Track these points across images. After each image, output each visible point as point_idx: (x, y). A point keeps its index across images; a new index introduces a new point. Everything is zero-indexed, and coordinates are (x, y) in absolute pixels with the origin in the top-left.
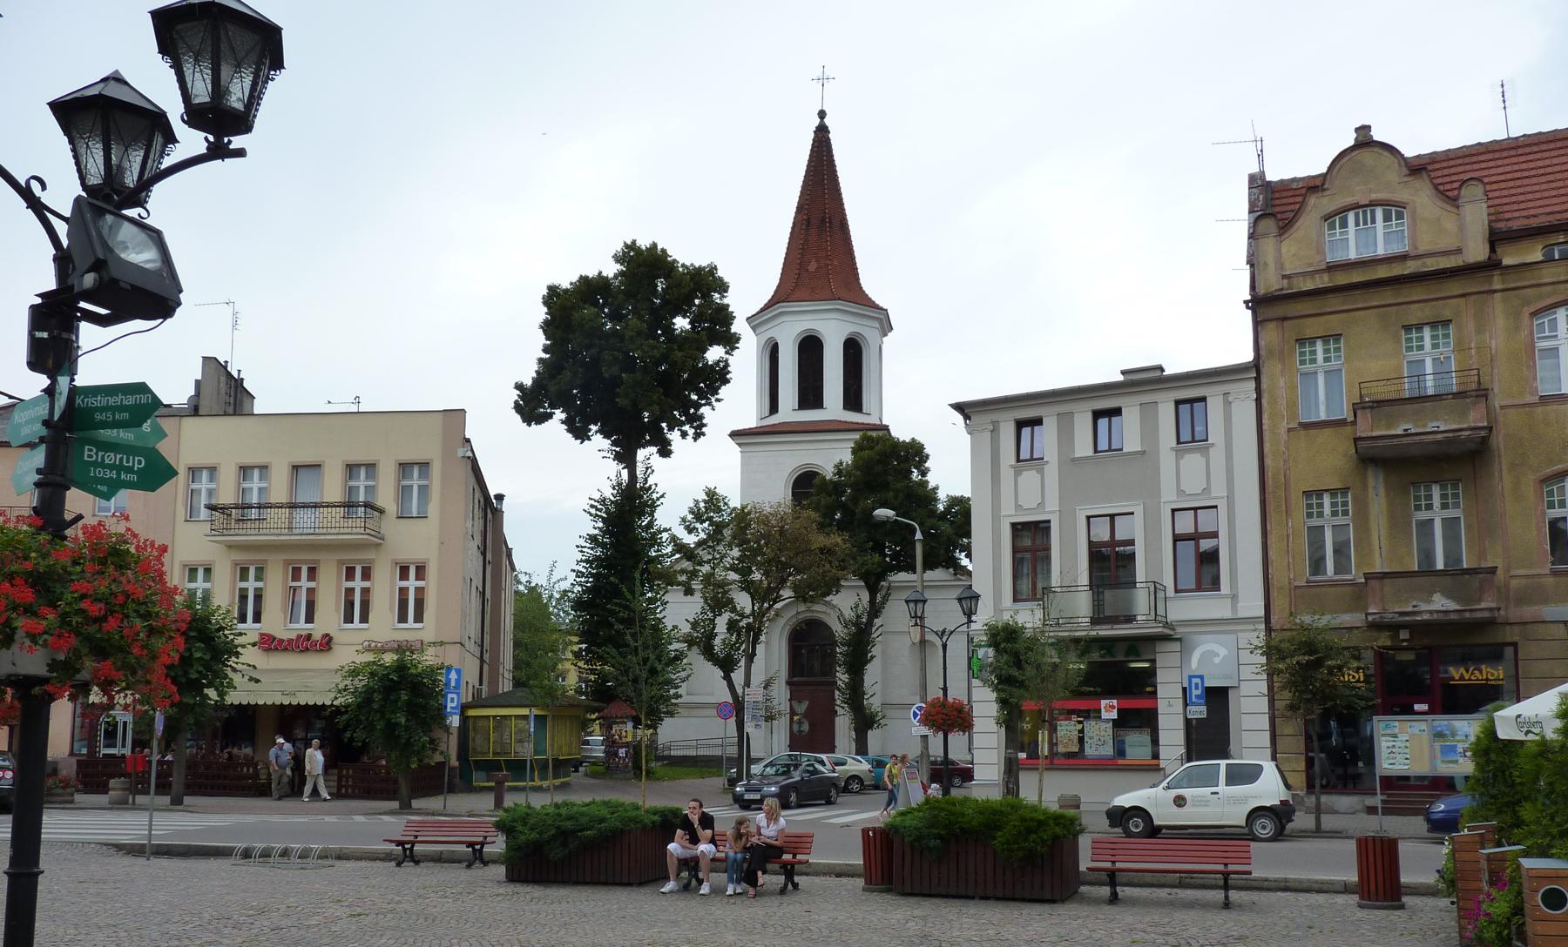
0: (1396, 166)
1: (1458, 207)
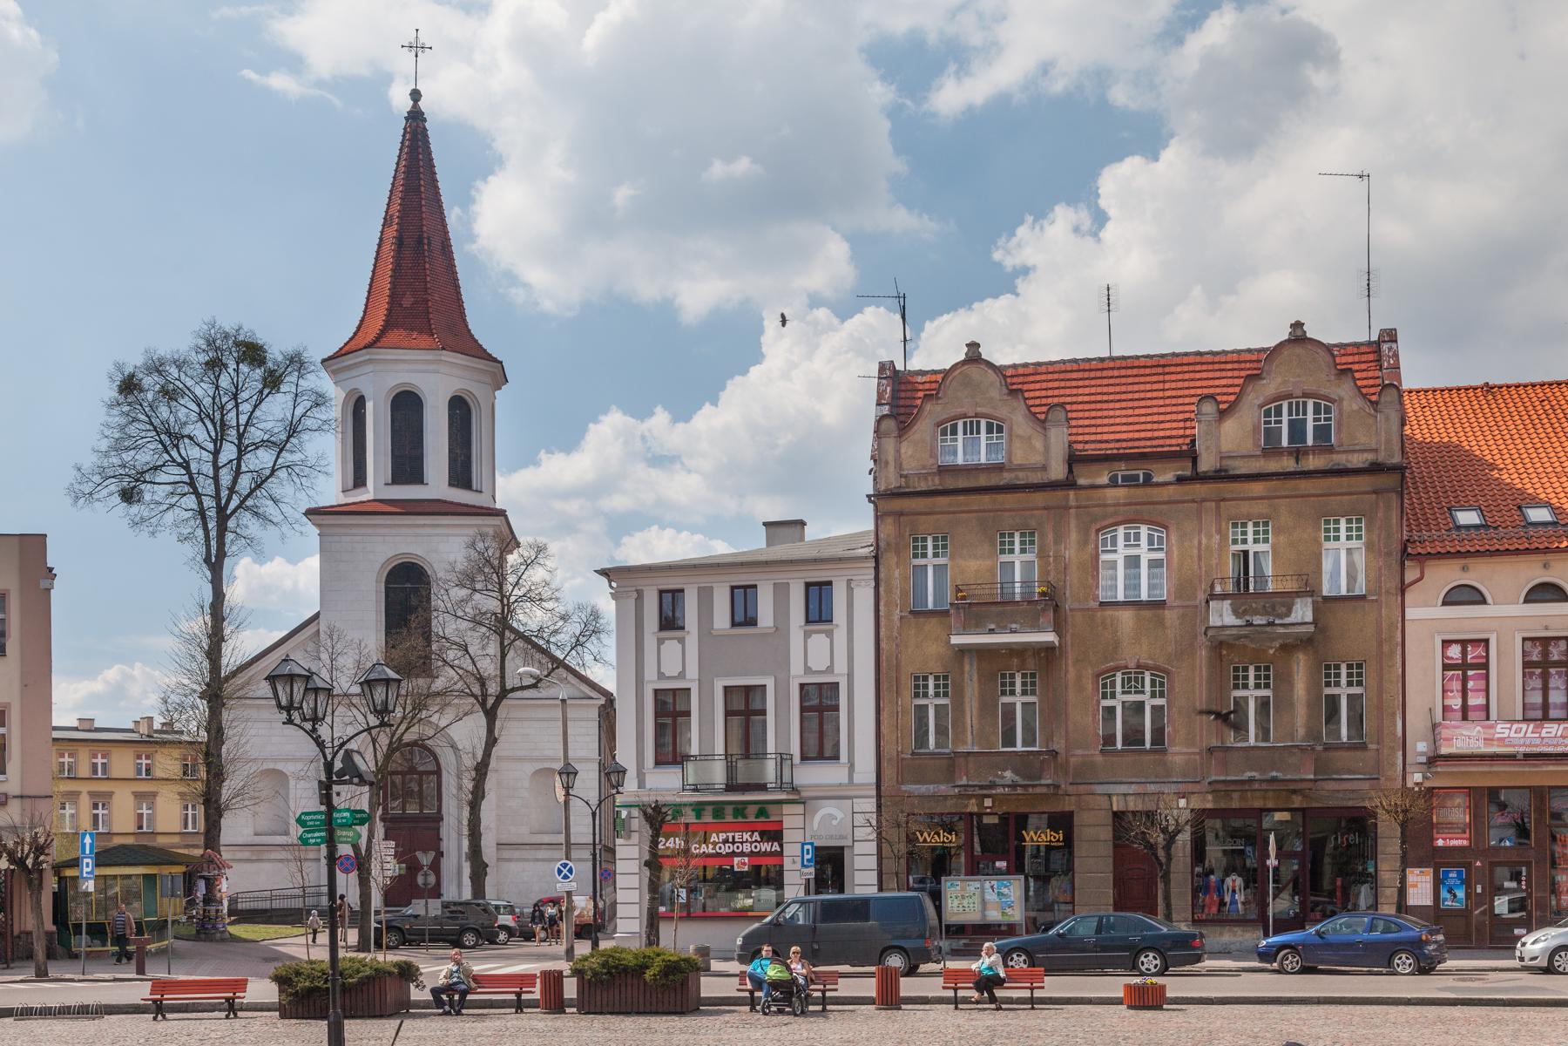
0: (998, 384)
1: (1045, 429)
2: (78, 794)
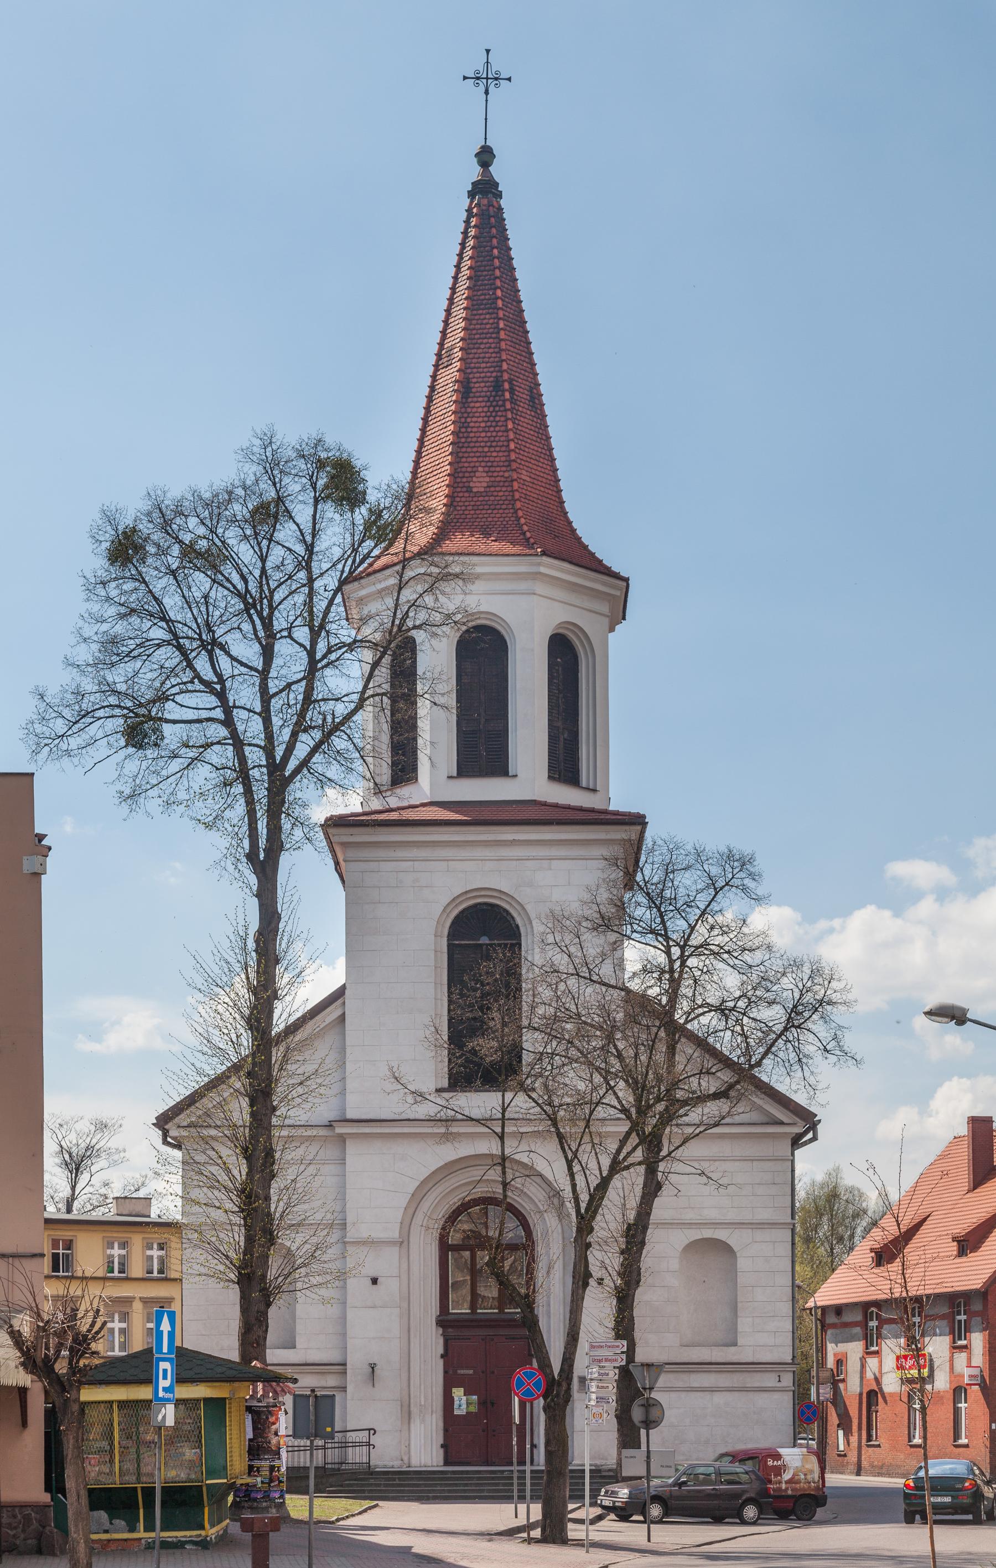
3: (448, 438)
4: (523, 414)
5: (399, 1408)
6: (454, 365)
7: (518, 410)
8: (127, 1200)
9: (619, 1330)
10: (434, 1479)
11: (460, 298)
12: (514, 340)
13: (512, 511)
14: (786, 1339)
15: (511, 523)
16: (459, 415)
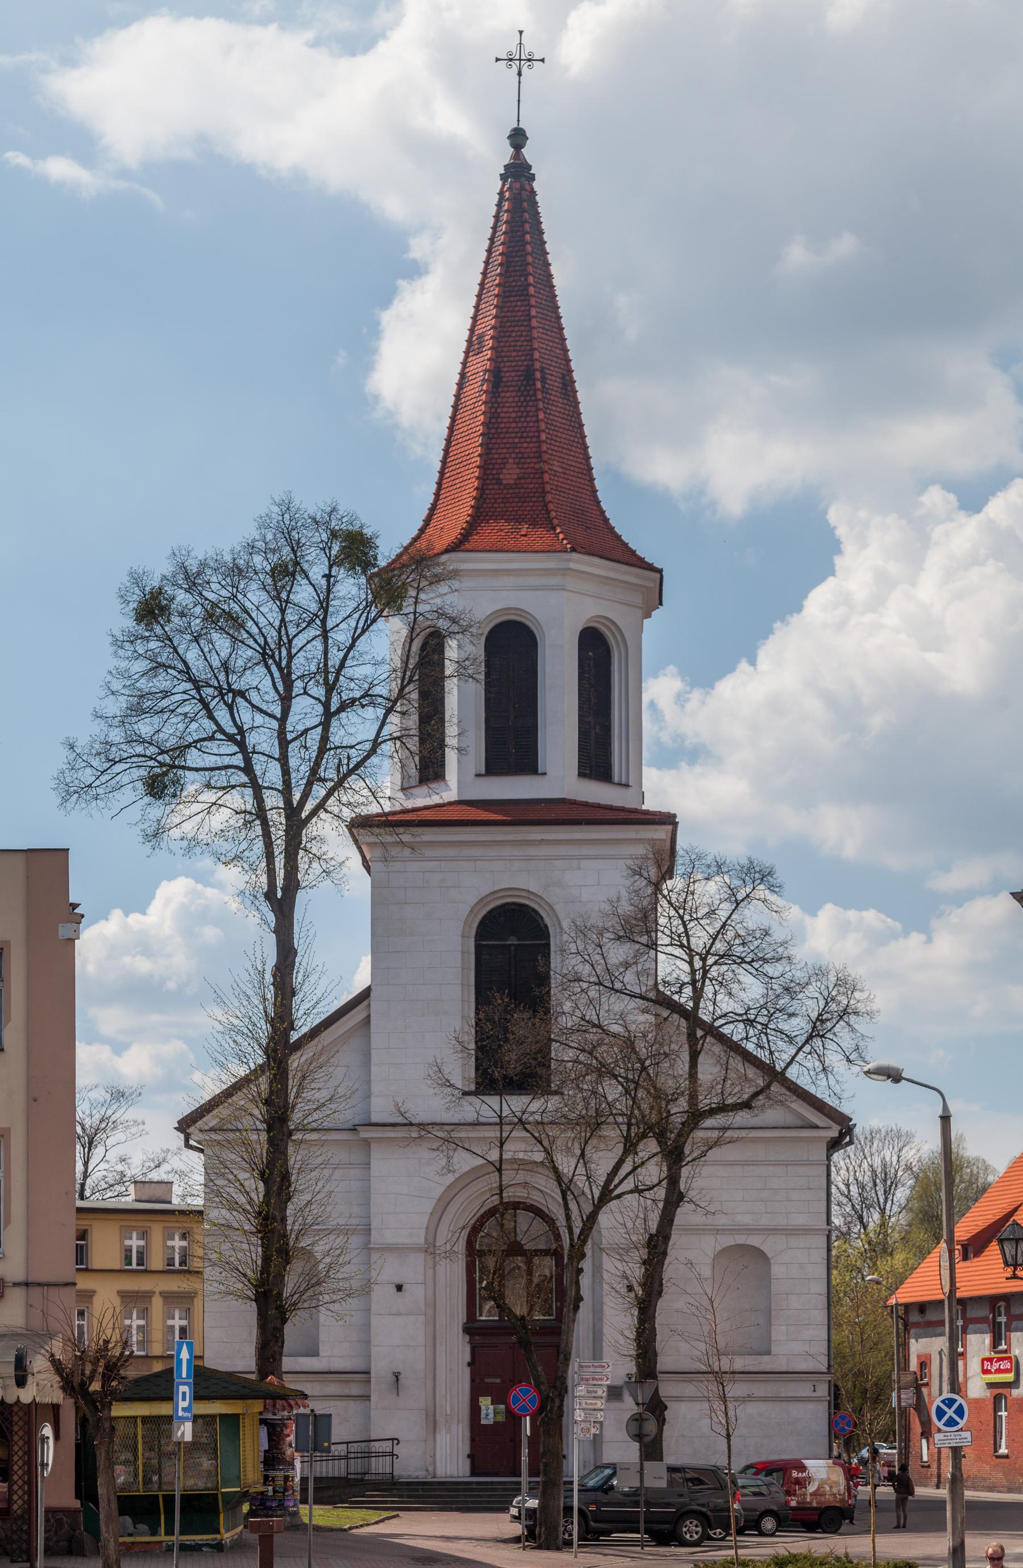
2: (145, 1297)
3: (478, 429)
4: (555, 403)
5: (424, 1417)
6: (485, 353)
7: (550, 399)
8: (146, 1185)
9: (640, 1341)
10: (458, 1490)
11: (491, 284)
12: (546, 327)
13: (542, 504)
14: (821, 1348)
15: (541, 516)
16: (490, 405)
